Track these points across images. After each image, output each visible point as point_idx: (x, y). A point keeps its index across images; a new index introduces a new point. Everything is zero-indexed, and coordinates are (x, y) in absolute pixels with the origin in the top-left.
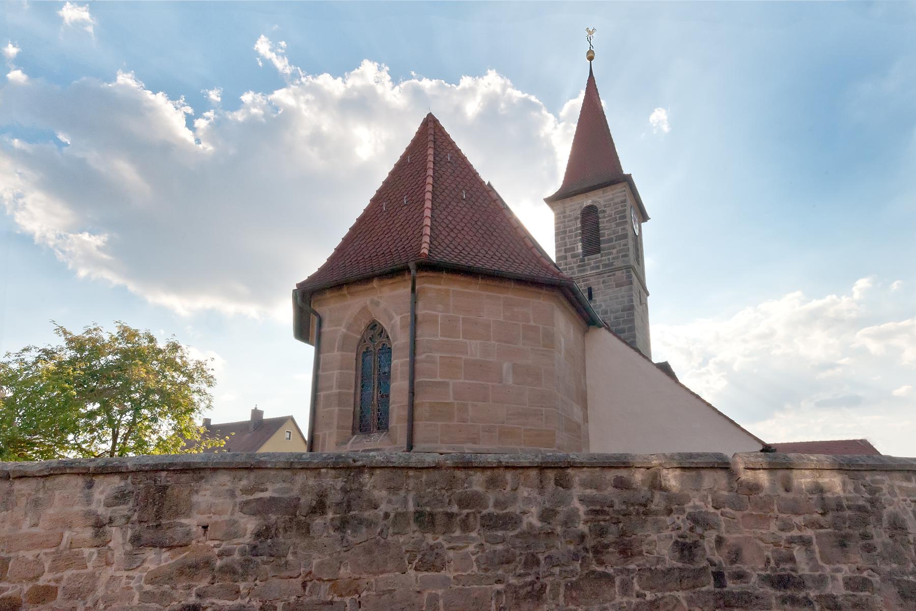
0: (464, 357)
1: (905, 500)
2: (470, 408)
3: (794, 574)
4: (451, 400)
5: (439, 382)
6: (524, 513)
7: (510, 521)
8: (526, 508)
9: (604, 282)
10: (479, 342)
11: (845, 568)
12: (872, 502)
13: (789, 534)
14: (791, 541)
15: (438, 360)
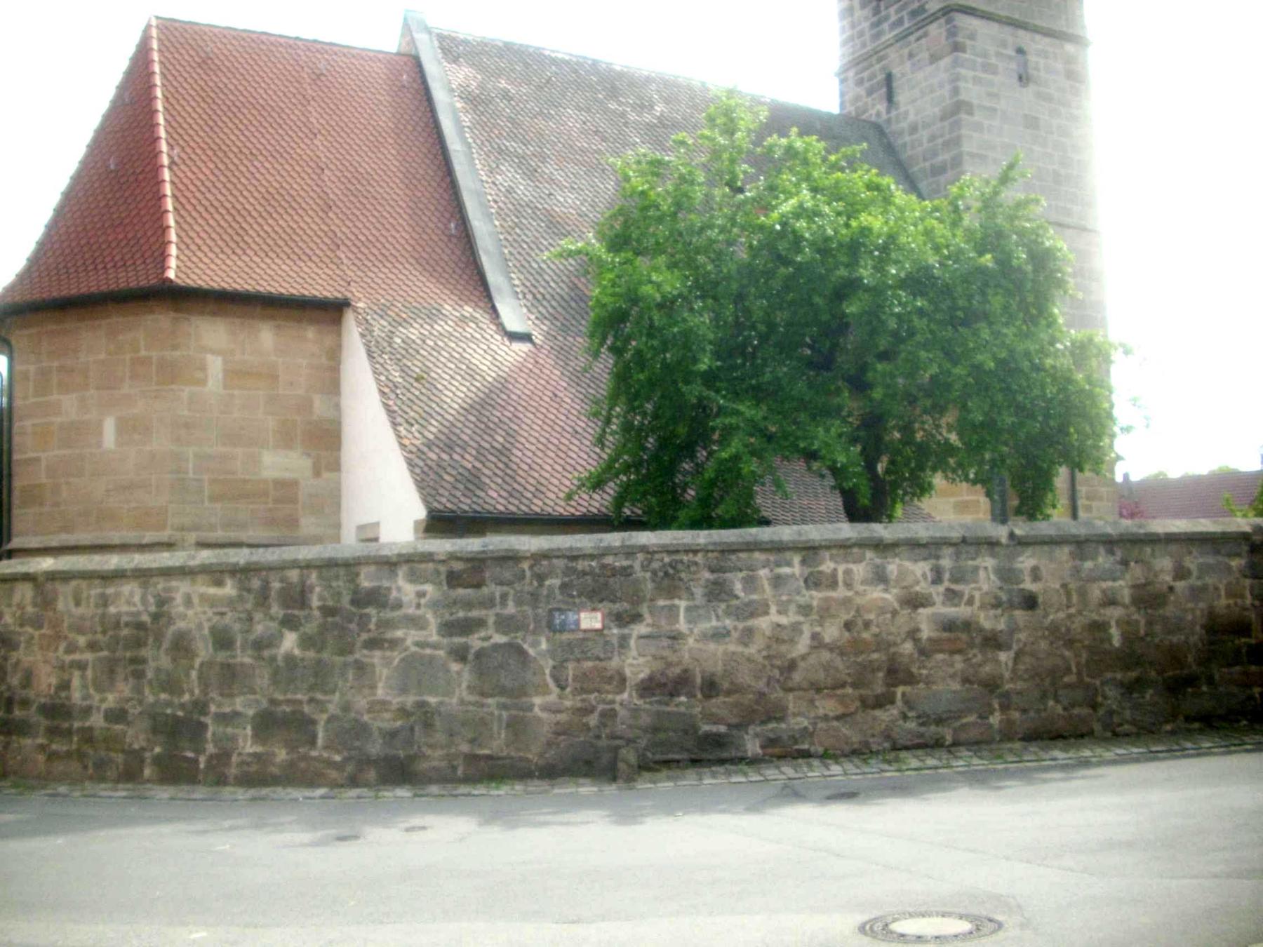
0: (59, 420)
1: (205, 613)
9: (911, 55)
10: (74, 395)
12: (156, 617)
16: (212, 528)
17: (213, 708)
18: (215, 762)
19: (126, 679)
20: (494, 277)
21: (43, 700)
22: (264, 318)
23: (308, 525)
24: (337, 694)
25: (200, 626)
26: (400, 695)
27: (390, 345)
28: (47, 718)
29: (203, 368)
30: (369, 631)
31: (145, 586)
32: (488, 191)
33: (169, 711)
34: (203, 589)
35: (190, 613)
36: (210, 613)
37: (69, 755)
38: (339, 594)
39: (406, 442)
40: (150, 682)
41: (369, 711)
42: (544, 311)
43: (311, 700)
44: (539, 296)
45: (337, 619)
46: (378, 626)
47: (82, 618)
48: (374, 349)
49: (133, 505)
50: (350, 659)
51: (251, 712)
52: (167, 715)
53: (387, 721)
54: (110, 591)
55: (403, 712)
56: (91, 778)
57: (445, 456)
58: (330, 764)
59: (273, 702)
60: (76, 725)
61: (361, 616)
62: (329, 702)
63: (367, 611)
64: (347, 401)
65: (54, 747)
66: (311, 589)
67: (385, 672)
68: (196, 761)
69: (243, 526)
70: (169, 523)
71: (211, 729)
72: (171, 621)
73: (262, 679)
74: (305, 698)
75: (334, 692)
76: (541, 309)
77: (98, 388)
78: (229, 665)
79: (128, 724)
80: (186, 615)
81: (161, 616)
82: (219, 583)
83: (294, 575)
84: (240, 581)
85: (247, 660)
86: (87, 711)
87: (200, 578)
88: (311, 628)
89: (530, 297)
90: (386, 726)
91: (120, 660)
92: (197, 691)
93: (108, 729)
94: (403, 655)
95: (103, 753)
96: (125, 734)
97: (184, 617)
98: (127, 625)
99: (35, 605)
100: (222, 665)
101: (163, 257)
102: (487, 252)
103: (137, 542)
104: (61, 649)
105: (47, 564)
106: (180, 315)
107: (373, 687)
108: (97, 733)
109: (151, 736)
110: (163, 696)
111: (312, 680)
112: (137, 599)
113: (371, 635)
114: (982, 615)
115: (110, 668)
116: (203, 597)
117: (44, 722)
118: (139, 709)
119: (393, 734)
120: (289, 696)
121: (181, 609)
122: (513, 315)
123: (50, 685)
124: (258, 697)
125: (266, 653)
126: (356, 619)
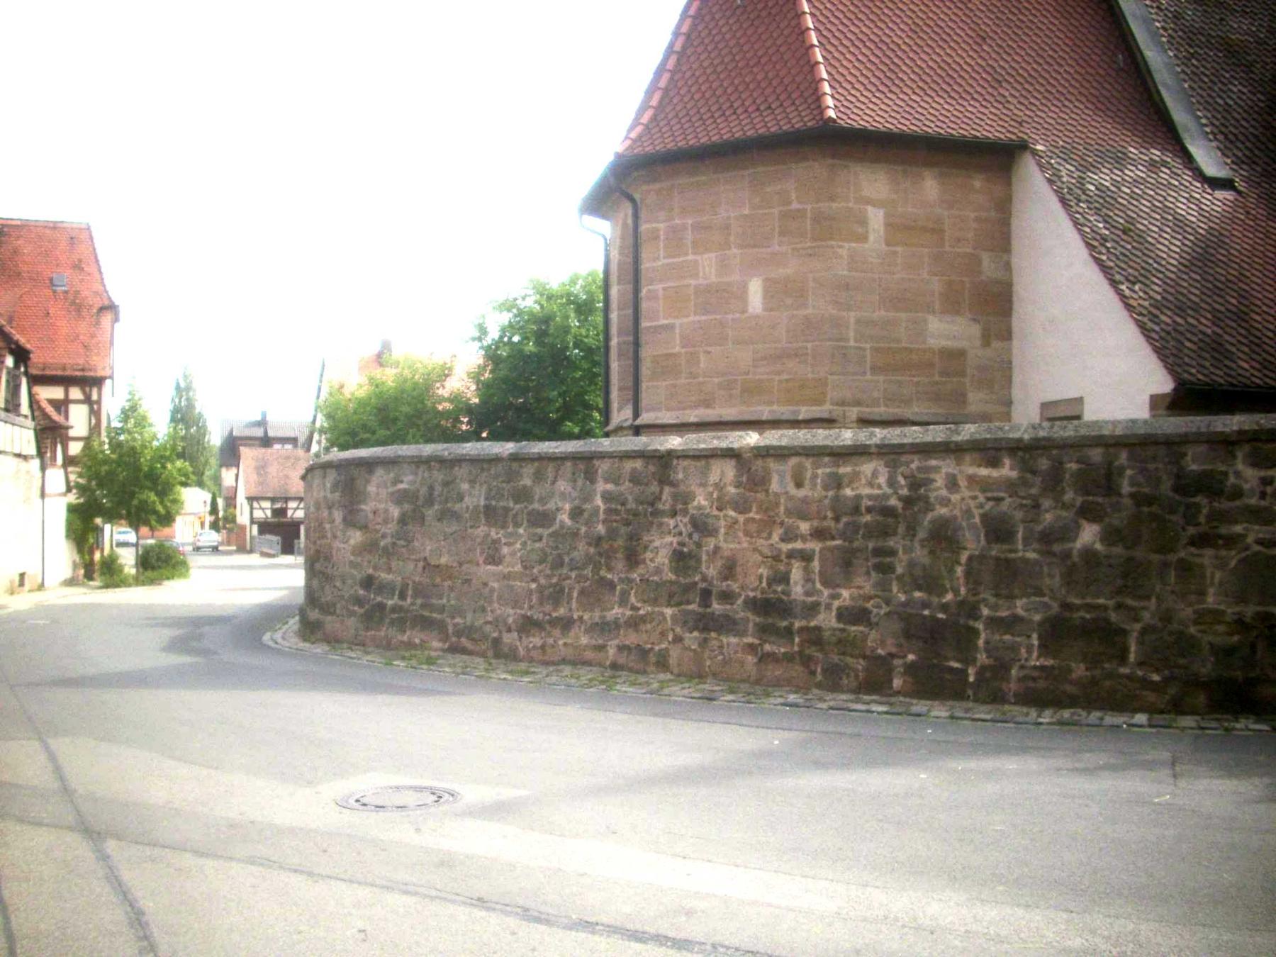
1: (975, 498)
2: (702, 358)
3: (785, 598)
4: (677, 349)
5: (662, 326)
6: (558, 510)
7: (543, 519)
8: (560, 504)
10: (713, 255)
11: (845, 593)
13: (790, 546)
14: (791, 555)
15: (661, 293)
16: (875, 402)
17: (985, 612)
18: (988, 675)
19: (868, 573)
20: (1179, 116)
21: (751, 594)
22: (929, 164)
23: (976, 400)
24: (1154, 600)
25: (968, 513)
26: (1237, 604)
27: (1084, 193)
28: (758, 614)
29: (863, 222)
30: (1198, 524)
31: (893, 466)
32: (1154, 17)
33: (926, 612)
34: (972, 470)
35: (955, 498)
36: (981, 499)
37: (789, 658)
38: (1159, 480)
39: (1131, 302)
40: (899, 578)
41: (1196, 623)
42: (1240, 154)
43: (1119, 606)
44: (1231, 136)
45: (1154, 508)
46: (1210, 518)
47: (805, 500)
48: (1068, 197)
49: (785, 377)
50: (1172, 558)
51: (1037, 618)
52: (925, 617)
53: (1220, 636)
54: (845, 470)
55: (1240, 624)
56: (819, 686)
57: (1179, 320)
58: (1146, 683)
59: (1066, 606)
60: (797, 624)
61: (1188, 506)
62: (1144, 608)
63: (1198, 499)
64: (1021, 258)
65: (767, 647)
66: (1121, 470)
67: (1218, 575)
68: (964, 672)
69: (907, 402)
70: (829, 397)
71: (983, 636)
72: (929, 507)
73: (1053, 579)
74: (1111, 603)
75: (1148, 598)
76: (1235, 151)
77: (741, 247)
78: (1007, 560)
79: (870, 625)
80: (949, 500)
81: (916, 498)
82: (994, 463)
83: (1096, 455)
84: (1023, 460)
85: (1032, 555)
86: (813, 609)
87: (968, 458)
88: (1118, 520)
89: (1220, 137)
90: (1218, 640)
91: (858, 550)
92: (963, 591)
93: (843, 630)
94: (1243, 555)
95: (836, 658)
96: (865, 637)
97: (945, 502)
98: (869, 510)
99: (738, 485)
100: (997, 559)
101: (818, 98)
102: (1165, 85)
103: (792, 418)
104: (775, 538)
105: (674, 442)
106: (836, 161)
107: (1202, 593)
108: (827, 634)
109: (902, 641)
110: (917, 594)
111: (1119, 582)
112: (882, 480)
113: (1202, 529)
114: (352, 542)
115: (846, 563)
116: (972, 479)
117: (754, 619)
118: (885, 609)
119: (1229, 651)
120: (1089, 600)
121: (944, 492)
122: (1209, 160)
123: (761, 577)
124: (1046, 599)
125: (1057, 548)
126: (1182, 509)
